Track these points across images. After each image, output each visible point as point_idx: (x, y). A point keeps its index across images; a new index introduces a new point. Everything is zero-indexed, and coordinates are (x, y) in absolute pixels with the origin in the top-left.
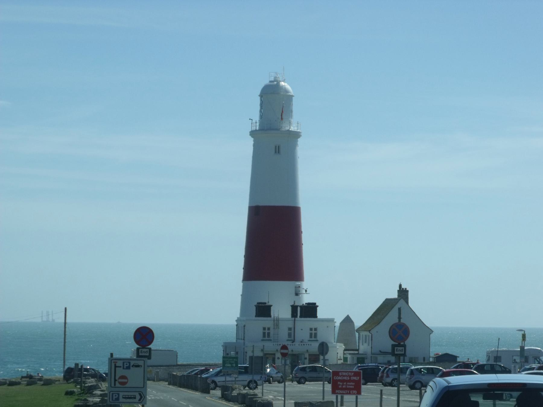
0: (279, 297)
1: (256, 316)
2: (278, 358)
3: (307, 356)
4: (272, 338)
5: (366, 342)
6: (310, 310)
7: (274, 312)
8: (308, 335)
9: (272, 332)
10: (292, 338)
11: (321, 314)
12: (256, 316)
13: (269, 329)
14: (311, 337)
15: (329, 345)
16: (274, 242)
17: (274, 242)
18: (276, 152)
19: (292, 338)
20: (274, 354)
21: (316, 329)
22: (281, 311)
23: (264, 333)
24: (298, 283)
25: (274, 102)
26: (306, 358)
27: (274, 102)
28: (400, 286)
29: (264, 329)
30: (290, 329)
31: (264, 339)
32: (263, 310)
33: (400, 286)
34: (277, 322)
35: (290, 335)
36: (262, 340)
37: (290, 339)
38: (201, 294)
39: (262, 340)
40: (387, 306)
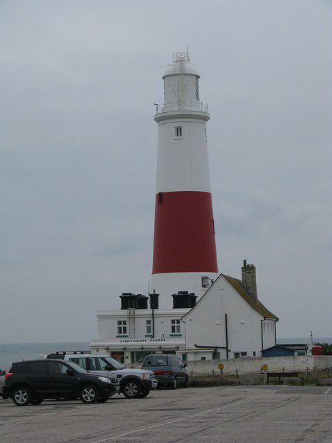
2: (127, 357)
8: (170, 329)
9: (127, 326)
10: (152, 334)
13: (178, 322)
17: (184, 228)
18: (181, 129)
19: (152, 334)
20: (122, 353)
23: (173, 327)
28: (245, 261)
29: (173, 322)
30: (148, 322)
31: (120, 335)
33: (245, 261)
35: (149, 330)
36: (171, 336)
37: (149, 334)
39: (171, 336)
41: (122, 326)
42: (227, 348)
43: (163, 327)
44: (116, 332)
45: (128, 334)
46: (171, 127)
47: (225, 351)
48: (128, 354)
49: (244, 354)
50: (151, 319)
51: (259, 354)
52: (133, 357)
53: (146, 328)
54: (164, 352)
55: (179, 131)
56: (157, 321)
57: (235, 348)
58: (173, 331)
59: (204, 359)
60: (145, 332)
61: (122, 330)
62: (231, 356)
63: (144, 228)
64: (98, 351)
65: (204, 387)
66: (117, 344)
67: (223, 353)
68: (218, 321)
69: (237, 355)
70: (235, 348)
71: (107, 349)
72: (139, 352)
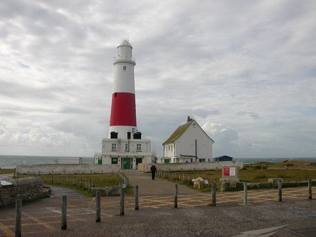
16: (124, 108)
17: (124, 108)
20: (117, 159)
21: (140, 145)
23: (138, 148)
29: (113, 145)
30: (126, 145)
33: (189, 117)
34: (120, 142)
35: (126, 148)
41: (114, 146)
42: (196, 157)
43: (133, 147)
44: (111, 149)
45: (117, 149)
46: (122, 65)
49: (204, 160)
52: (122, 160)
54: (288, 165)
55: (125, 68)
56: (131, 144)
57: (199, 157)
59: (187, 162)
61: (114, 149)
62: (198, 160)
63: (107, 110)
66: (115, 154)
67: (194, 159)
68: (192, 143)
69: (200, 160)
70: (199, 157)
72: (126, 158)
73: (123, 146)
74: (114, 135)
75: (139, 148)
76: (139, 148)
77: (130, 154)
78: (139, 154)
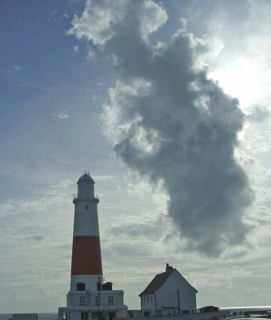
0: (89, 281)
1: (78, 290)
3: (108, 313)
4: (85, 303)
5: (148, 301)
6: (109, 286)
7: (87, 287)
9: (85, 299)
10: (98, 303)
11: (114, 288)
12: (78, 290)
13: (84, 297)
14: (109, 302)
15: (209, 52)
16: (86, 253)
17: (86, 253)
19: (98, 303)
21: (112, 297)
22: (91, 287)
23: (81, 300)
24: (100, 276)
25: (86, 183)
26: (107, 315)
27: (86, 183)
28: (167, 265)
29: (81, 298)
30: (96, 297)
32: (81, 287)
33: (167, 265)
34: (89, 294)
35: (97, 301)
36: (80, 305)
38: (55, 286)
40: (159, 280)
42: (179, 308)
45: (85, 303)
47: (178, 310)
48: (90, 314)
49: (188, 312)
50: (98, 295)
51: (202, 311)
53: (95, 301)
56: (101, 297)
57: (183, 308)
58: (81, 302)
60: (95, 302)
61: (82, 302)
62: (181, 312)
64: (74, 312)
65: (27, 314)
66: (84, 308)
69: (184, 312)
71: (80, 311)
73: (93, 301)
74: (81, 287)
75: (111, 301)
76: (111, 301)
77: (101, 308)
78: (112, 308)
